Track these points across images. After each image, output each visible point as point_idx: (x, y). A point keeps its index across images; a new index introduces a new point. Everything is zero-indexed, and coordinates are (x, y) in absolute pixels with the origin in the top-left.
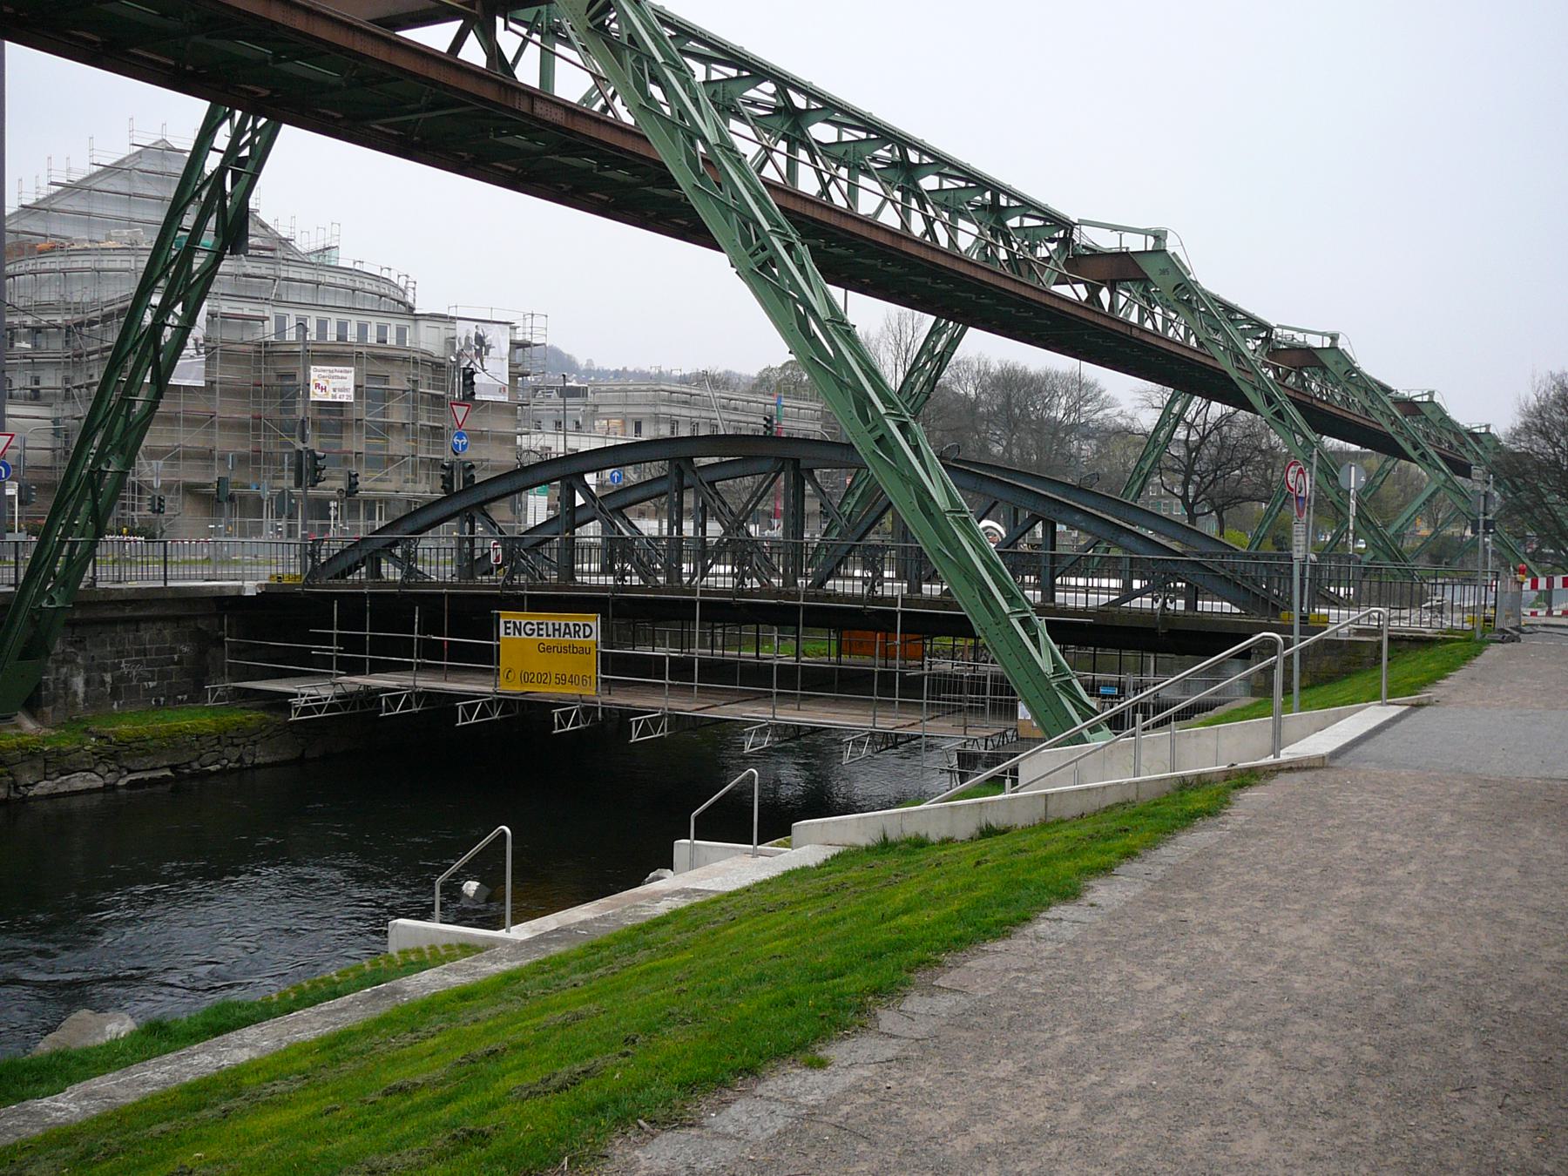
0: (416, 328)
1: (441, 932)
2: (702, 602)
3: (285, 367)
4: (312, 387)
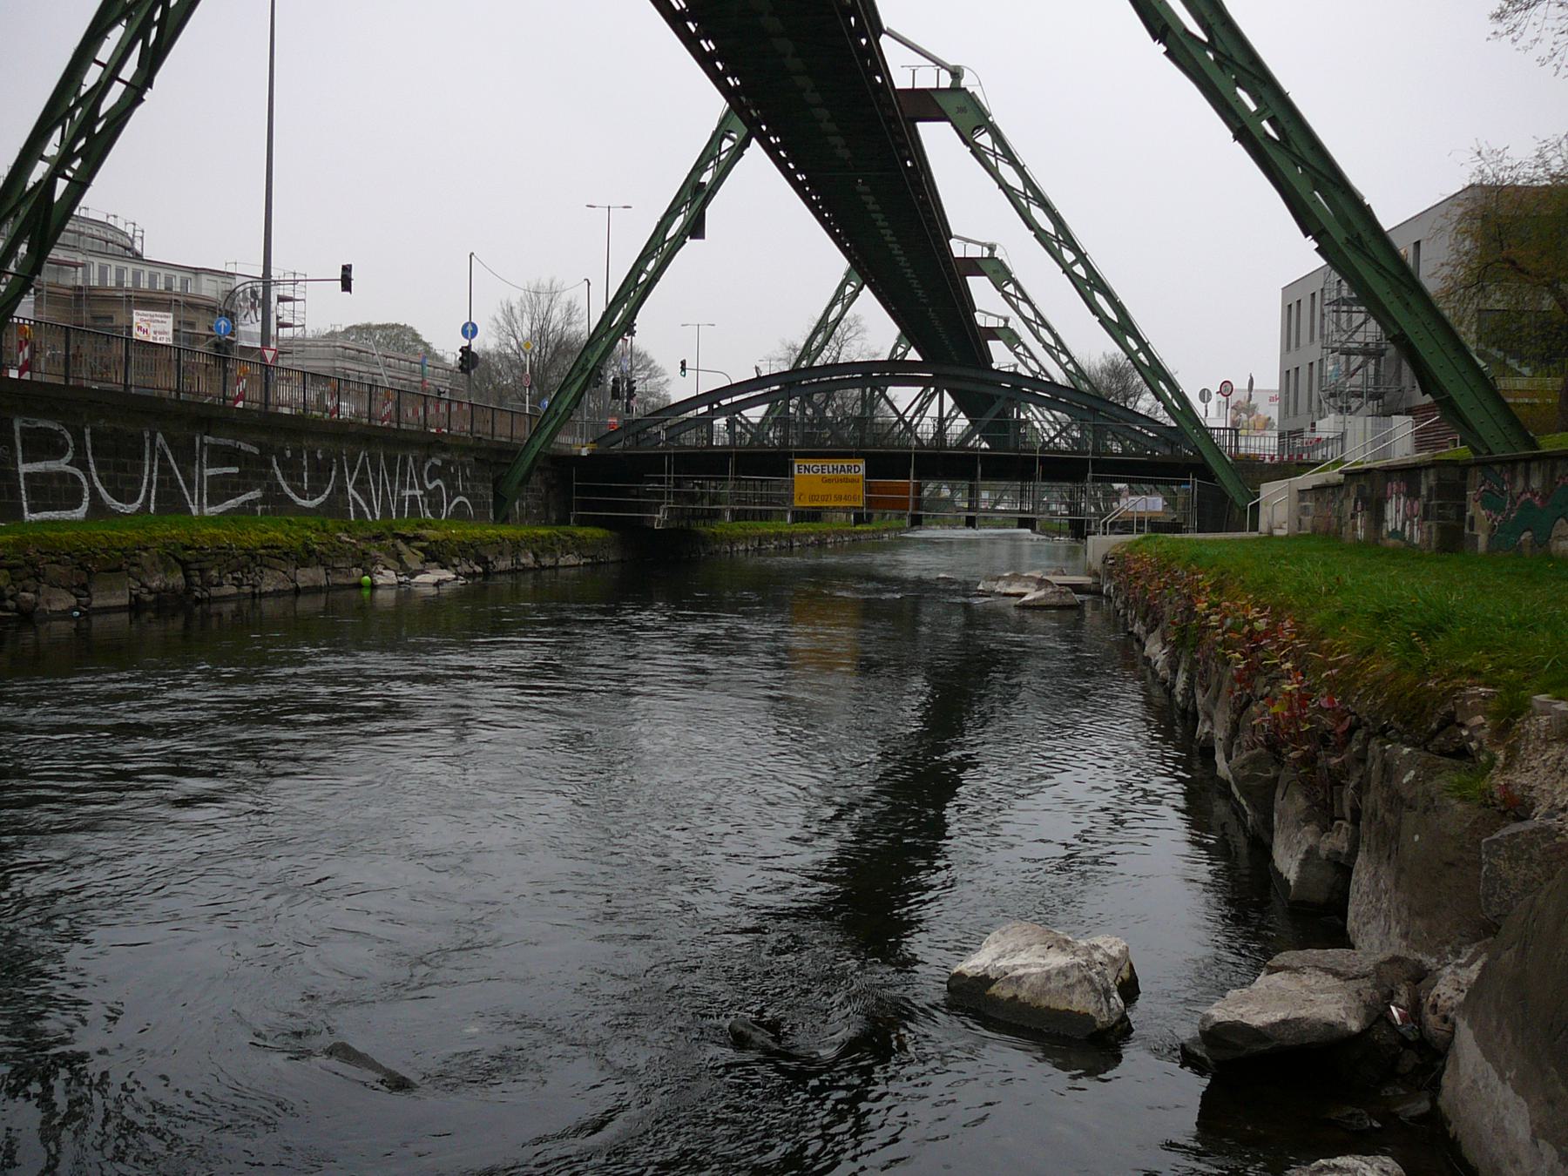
0: (197, 280)
1: (1199, 543)
2: (916, 454)
3: (102, 310)
4: (135, 329)
